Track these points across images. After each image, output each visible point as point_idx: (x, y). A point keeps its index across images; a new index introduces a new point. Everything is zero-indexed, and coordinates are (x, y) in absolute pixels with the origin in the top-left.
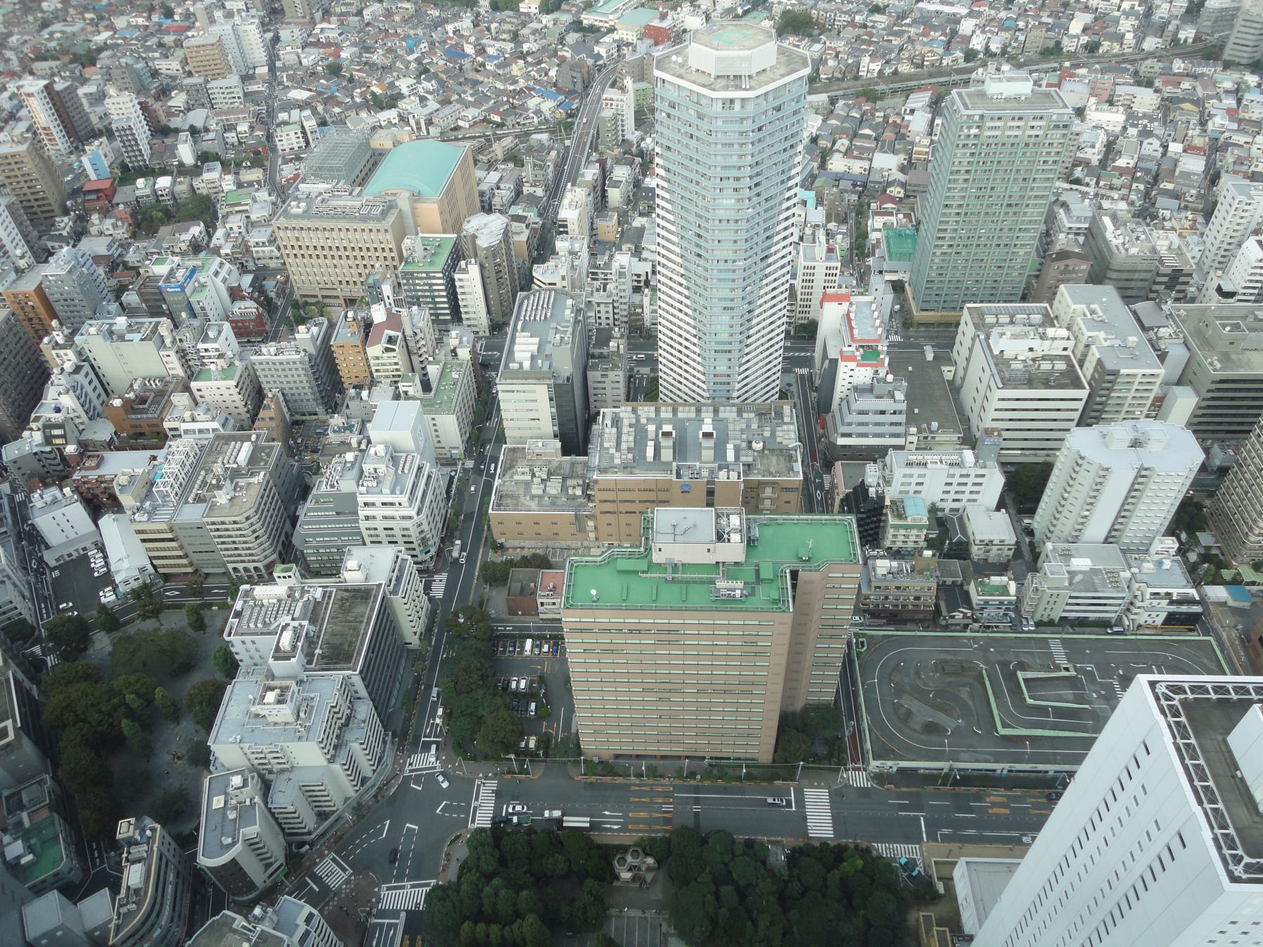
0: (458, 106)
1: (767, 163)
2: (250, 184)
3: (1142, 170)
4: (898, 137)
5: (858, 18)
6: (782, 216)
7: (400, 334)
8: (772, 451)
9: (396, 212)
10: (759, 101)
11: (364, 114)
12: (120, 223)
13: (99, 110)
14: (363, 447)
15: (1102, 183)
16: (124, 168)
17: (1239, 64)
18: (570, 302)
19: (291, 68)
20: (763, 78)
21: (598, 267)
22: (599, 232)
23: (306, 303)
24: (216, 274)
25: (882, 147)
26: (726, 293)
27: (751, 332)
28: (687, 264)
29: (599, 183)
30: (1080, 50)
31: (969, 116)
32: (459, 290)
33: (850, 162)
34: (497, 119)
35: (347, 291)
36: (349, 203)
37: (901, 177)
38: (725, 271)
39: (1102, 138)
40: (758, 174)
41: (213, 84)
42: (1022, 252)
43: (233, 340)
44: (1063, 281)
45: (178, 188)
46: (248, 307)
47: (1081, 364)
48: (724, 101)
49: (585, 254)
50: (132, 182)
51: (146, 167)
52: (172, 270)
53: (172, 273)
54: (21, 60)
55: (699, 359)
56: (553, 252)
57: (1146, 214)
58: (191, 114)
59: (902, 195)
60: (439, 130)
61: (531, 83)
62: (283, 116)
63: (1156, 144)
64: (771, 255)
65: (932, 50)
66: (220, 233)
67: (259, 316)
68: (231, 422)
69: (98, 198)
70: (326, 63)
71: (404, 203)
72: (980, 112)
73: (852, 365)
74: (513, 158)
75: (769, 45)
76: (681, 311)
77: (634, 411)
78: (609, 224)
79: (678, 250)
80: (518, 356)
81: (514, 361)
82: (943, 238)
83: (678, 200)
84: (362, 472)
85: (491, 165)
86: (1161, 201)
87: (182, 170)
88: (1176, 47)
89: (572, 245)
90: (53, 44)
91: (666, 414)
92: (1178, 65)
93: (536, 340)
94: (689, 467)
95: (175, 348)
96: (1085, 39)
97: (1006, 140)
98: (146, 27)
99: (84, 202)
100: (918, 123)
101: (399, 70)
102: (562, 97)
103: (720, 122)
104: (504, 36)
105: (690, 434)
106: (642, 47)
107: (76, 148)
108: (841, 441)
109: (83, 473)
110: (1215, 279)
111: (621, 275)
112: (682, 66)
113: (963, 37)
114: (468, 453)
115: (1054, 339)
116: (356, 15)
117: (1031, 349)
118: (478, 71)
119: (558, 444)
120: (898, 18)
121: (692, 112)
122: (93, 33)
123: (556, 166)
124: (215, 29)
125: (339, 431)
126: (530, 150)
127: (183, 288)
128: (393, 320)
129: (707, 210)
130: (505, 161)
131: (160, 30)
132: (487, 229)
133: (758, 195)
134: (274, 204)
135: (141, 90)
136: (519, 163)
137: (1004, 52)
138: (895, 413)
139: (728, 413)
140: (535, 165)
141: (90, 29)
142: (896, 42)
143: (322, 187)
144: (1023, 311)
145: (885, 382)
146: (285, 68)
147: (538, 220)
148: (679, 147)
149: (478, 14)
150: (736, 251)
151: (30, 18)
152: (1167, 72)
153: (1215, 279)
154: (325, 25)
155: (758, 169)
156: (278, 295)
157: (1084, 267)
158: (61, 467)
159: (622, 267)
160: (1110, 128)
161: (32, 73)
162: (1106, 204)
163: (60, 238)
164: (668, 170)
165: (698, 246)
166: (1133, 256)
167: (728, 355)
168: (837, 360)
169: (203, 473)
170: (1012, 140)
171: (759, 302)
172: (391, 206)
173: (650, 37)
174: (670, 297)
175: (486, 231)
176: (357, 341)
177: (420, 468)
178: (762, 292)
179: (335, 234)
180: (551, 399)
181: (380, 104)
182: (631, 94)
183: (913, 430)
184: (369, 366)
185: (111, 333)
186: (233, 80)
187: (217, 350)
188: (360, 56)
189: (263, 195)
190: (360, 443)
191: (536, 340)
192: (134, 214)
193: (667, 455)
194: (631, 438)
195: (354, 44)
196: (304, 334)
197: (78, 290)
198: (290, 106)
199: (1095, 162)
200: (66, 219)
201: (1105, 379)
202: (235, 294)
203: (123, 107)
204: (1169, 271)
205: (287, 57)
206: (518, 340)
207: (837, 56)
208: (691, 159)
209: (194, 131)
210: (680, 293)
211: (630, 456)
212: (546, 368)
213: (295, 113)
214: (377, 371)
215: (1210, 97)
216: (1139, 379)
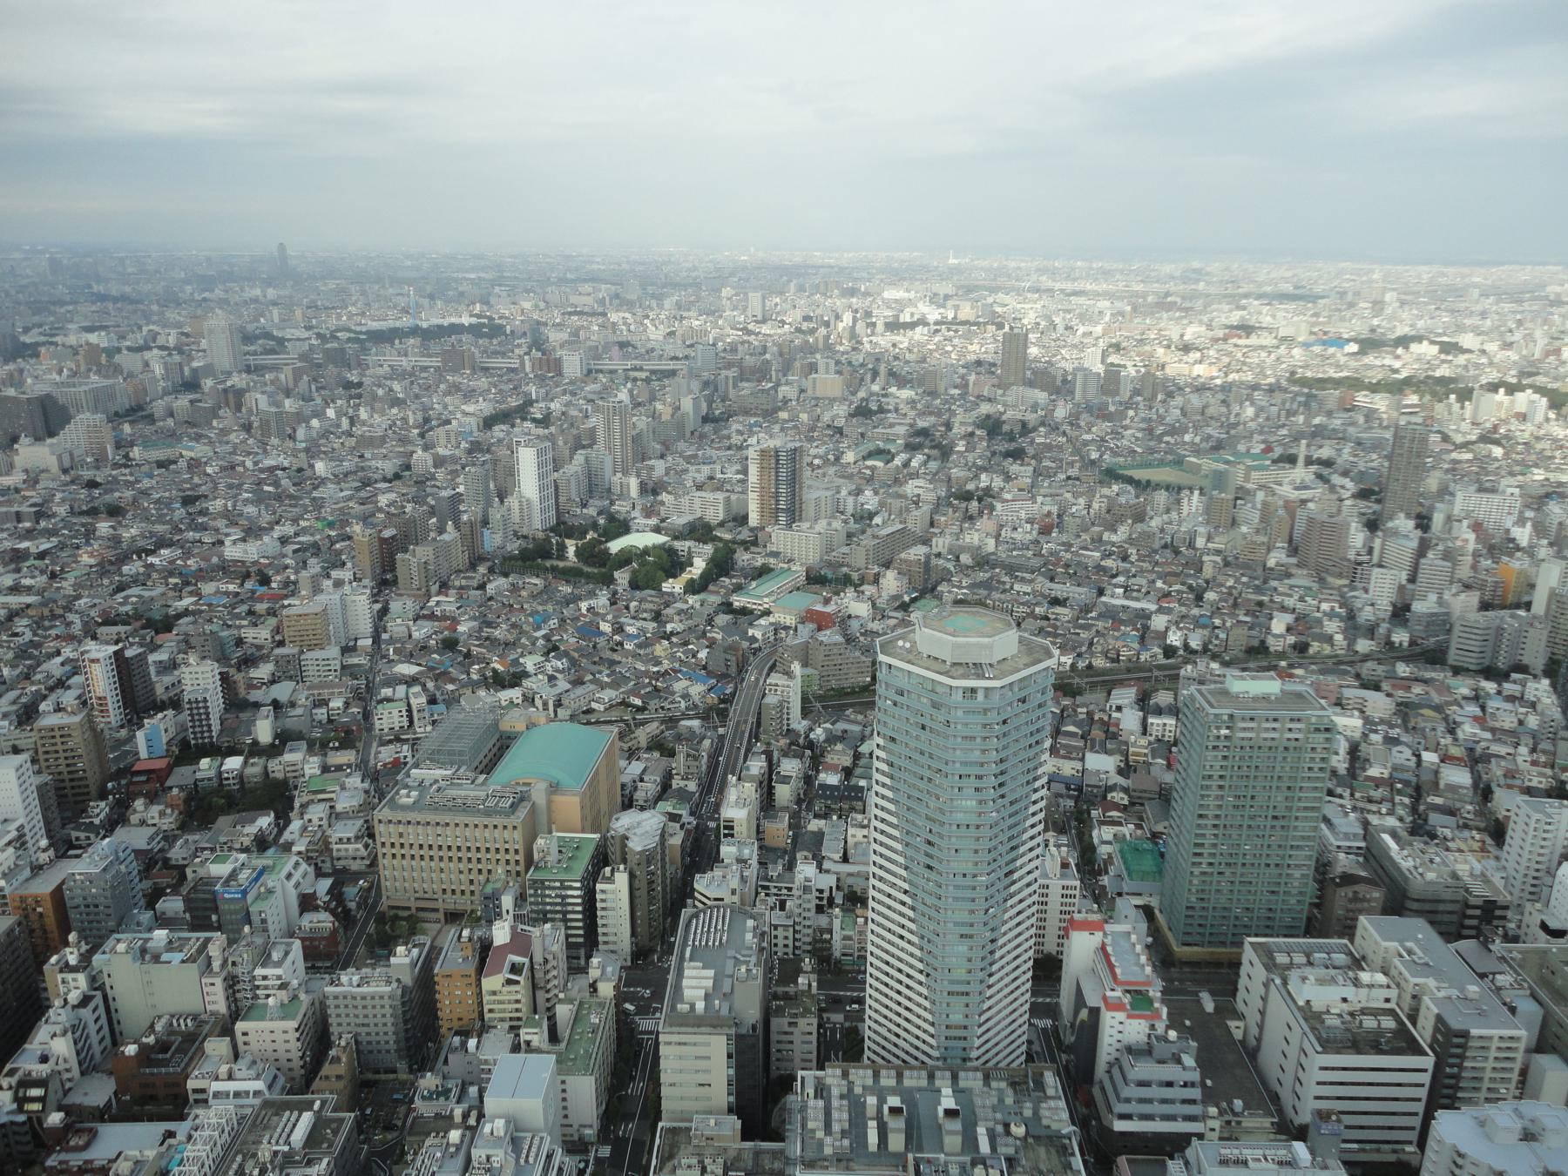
0: (592, 687)
1: (1013, 760)
2: (339, 768)
4: (1109, 737)
6: (1029, 823)
7: (526, 960)
8: (1037, 1138)
11: (482, 693)
12: (169, 811)
13: (168, 680)
14: (472, 1121)
15: (1357, 795)
16: (184, 744)
17: (1468, 670)
18: (750, 923)
20: (1005, 666)
23: (396, 918)
24: (289, 876)
26: (964, 916)
27: (995, 968)
28: (912, 877)
30: (1289, 650)
32: (599, 905)
34: (638, 702)
35: (450, 903)
36: (473, 794)
37: (1120, 780)
38: (964, 887)
40: (1002, 773)
43: (301, 964)
44: (1361, 911)
45: (250, 771)
46: (322, 921)
47: (1413, 1019)
49: (754, 862)
50: (195, 760)
51: (212, 744)
52: (234, 870)
53: (233, 875)
54: (85, 624)
55: (927, 1004)
57: (1420, 829)
58: (276, 686)
60: (569, 712)
61: (677, 665)
62: (386, 692)
63: (1408, 753)
64: (1015, 870)
66: (296, 825)
67: (334, 932)
68: (281, 1081)
69: (148, 781)
71: (539, 794)
73: (1121, 1016)
74: (659, 746)
76: (902, 937)
77: (845, 1075)
78: (779, 826)
80: (687, 993)
81: (683, 1002)
82: (1200, 854)
83: (903, 800)
84: (468, 1160)
85: (632, 754)
87: (255, 750)
88: (1391, 652)
91: (888, 1080)
92: (1403, 669)
93: (711, 973)
94: (929, 1161)
95: (224, 974)
96: (1291, 639)
97: (1262, 743)
98: (237, 594)
99: (128, 785)
100: (1129, 720)
101: (524, 646)
102: (714, 681)
103: (960, 713)
105: (922, 1110)
107: (129, 721)
108: (1120, 1126)
109: (63, 1156)
110: (1535, 913)
111: (806, 889)
112: (909, 651)
113: (1157, 632)
114: (604, 1135)
115: (1371, 986)
117: (1345, 1000)
119: (735, 1123)
121: (924, 700)
125: (430, 1098)
126: (679, 738)
127: (245, 893)
128: (520, 942)
129: (942, 811)
130: (649, 749)
132: (642, 829)
133: (1002, 796)
134: (367, 792)
135: (222, 659)
137: (1205, 650)
138: (1185, 1085)
139: (973, 1081)
141: (171, 593)
142: (1084, 635)
144: (1321, 949)
145: (1166, 1040)
146: (391, 641)
147: (691, 819)
148: (906, 739)
149: (615, 593)
150: (976, 864)
151: (106, 581)
152: (1391, 676)
153: (1535, 913)
155: (1003, 767)
156: (359, 906)
158: (29, 1148)
159: (808, 880)
160: (1348, 733)
161: (94, 637)
163: (90, 827)
164: (891, 765)
165: (927, 855)
166: (1430, 883)
167: (965, 999)
168: (1098, 1009)
169: (239, 1158)
170: (1269, 743)
171: (1003, 929)
172: (523, 798)
173: (812, 620)
174: (887, 918)
176: (471, 969)
177: (549, 1157)
178: (1007, 916)
179: (449, 831)
180: (729, 1056)
181: (500, 682)
183: (1213, 1111)
184: (481, 1004)
185: (143, 951)
186: (333, 651)
187: (279, 977)
189: (355, 781)
190: (466, 1116)
191: (711, 973)
192: (187, 801)
193: (896, 1142)
194: (845, 1116)
195: (474, 618)
196: (402, 956)
197: (108, 894)
198: (394, 681)
200: (102, 804)
201: (1451, 1044)
202: (307, 903)
203: (200, 678)
204: (1479, 902)
206: (687, 973)
208: (922, 753)
209: (276, 704)
210: (903, 915)
211: (846, 1142)
212: (724, 1012)
213: (401, 690)
214: (491, 1011)
215: (1449, 704)
216: (1496, 1043)
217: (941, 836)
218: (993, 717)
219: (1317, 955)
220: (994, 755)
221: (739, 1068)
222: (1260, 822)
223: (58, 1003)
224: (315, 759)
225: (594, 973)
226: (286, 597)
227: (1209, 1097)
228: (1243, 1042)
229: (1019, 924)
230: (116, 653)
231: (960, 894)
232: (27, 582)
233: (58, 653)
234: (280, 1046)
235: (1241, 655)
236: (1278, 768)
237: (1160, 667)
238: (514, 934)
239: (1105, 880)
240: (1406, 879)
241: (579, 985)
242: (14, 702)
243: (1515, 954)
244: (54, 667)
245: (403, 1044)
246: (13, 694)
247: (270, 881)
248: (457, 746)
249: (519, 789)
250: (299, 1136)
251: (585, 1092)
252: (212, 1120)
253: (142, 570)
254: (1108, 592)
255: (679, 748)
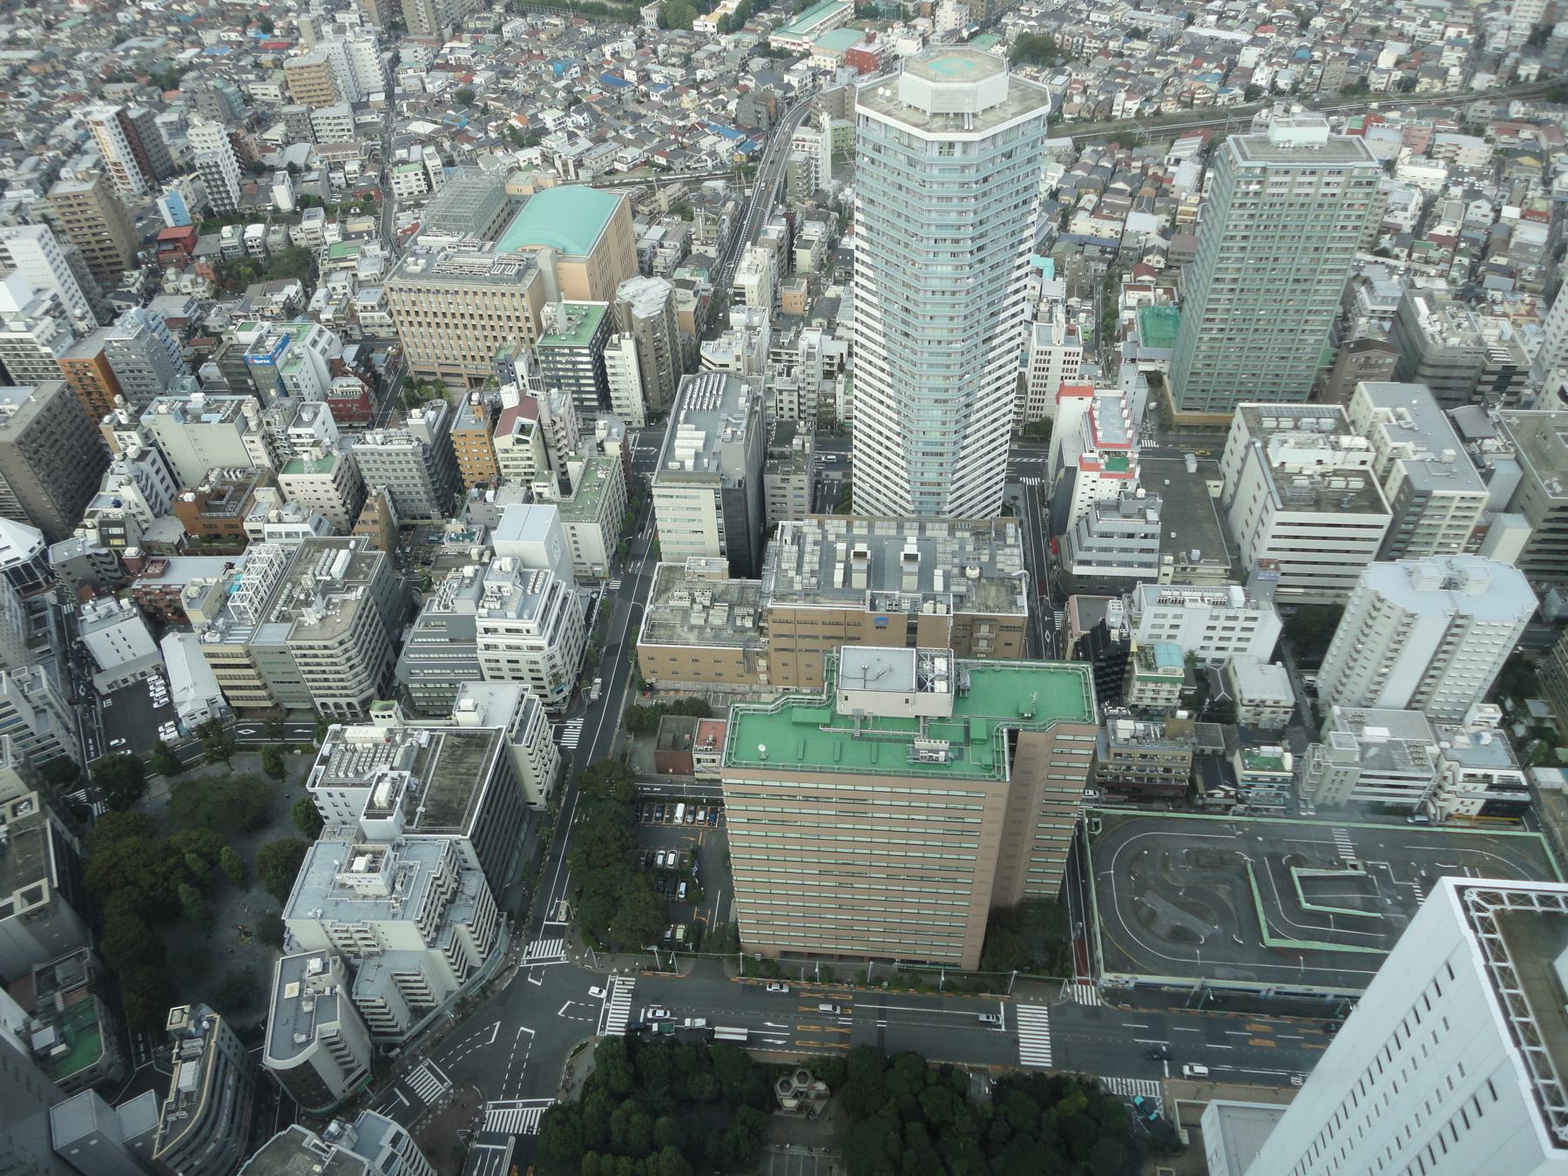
0: (615, 145)
2: (359, 235)
3: (1467, 240)
4: (1159, 193)
5: (1112, 45)
7: (535, 422)
9: (534, 272)
10: (984, 145)
11: (499, 153)
12: (200, 280)
13: (180, 142)
14: (485, 559)
15: (1415, 256)
16: (208, 213)
18: (745, 388)
19: (412, 95)
20: (990, 116)
21: (782, 347)
22: (783, 303)
23: (422, 382)
25: (1139, 205)
26: (940, 383)
27: (969, 431)
28: (892, 345)
29: (786, 242)
31: (1248, 169)
32: (609, 371)
33: (1099, 223)
34: (662, 161)
35: (473, 368)
37: (1162, 243)
38: (938, 354)
39: (1417, 199)
40: (982, 236)
41: (318, 113)
42: (1311, 339)
44: (1363, 377)
45: (272, 238)
46: (352, 385)
47: (1383, 481)
48: (942, 145)
49: (765, 330)
51: (234, 212)
52: (261, 337)
53: (260, 342)
54: (90, 81)
55: (903, 463)
56: (726, 325)
57: (1471, 295)
58: (290, 149)
59: (1162, 265)
60: (590, 173)
61: (705, 118)
62: (401, 153)
63: (1486, 207)
64: (996, 336)
65: (1204, 86)
66: (320, 293)
67: (365, 396)
68: (326, 524)
69: (176, 249)
70: (455, 89)
71: (544, 262)
72: (1262, 164)
73: (1095, 475)
74: (681, 209)
75: (999, 76)
76: (882, 402)
77: (821, 525)
78: (797, 293)
79: (880, 327)
80: (678, 452)
82: (1213, 320)
83: (882, 266)
84: (482, 590)
85: (653, 218)
86: (1491, 280)
87: (277, 216)
88: (1515, 86)
89: (750, 317)
90: (128, 63)
92: (1517, 109)
93: (702, 434)
95: (261, 433)
96: (1398, 75)
97: (1293, 199)
99: (157, 253)
100: (1184, 176)
101: (544, 99)
102: (743, 136)
103: (936, 171)
104: (674, 60)
105: (888, 554)
106: (843, 77)
107: (152, 188)
108: (1078, 570)
109: (145, 581)
111: (810, 356)
112: (890, 100)
114: (614, 570)
115: (1349, 449)
116: (494, 32)
117: (1320, 462)
118: (640, 103)
119: (725, 563)
120: (1162, 45)
121: (901, 157)
122: (176, 50)
123: (733, 221)
124: (323, 47)
125: (457, 540)
126: (702, 201)
127: (273, 359)
128: (527, 405)
129: (917, 277)
130: (671, 213)
131: (257, 47)
133: (981, 261)
135: (231, 119)
136: (688, 216)
137: (1295, 89)
138: (1146, 537)
139: (937, 531)
140: (707, 219)
141: (173, 45)
142: (1159, 74)
143: (446, 240)
144: (1311, 414)
145: (1135, 497)
147: (709, 286)
149: (643, 33)
150: (952, 330)
151: (103, 32)
152: (1502, 117)
154: (455, 44)
155: (981, 230)
156: (388, 371)
157: (1389, 360)
158: (119, 574)
160: (1427, 187)
161: (102, 97)
162: (1420, 282)
163: (128, 296)
164: (870, 228)
165: (905, 322)
166: (1453, 348)
167: (939, 459)
169: (289, 585)
170: (1301, 200)
171: (980, 394)
172: (529, 266)
174: (869, 385)
175: (644, 298)
176: (483, 428)
177: (554, 588)
178: (983, 382)
179: (459, 298)
180: (718, 508)
181: (520, 140)
182: (828, 134)
185: (184, 412)
186: (343, 108)
187: (312, 436)
188: (497, 82)
189: (374, 249)
190: (481, 555)
191: (702, 434)
192: (217, 269)
193: (859, 580)
194: (816, 559)
195: (490, 68)
197: (147, 359)
199: (1407, 229)
200: (136, 274)
201: (1413, 501)
202: (336, 368)
203: (208, 140)
204: (1498, 368)
205: (409, 82)
206: (679, 434)
207: (1085, 91)
208: (899, 215)
209: (293, 170)
210: (881, 380)
211: (814, 580)
212: (713, 469)
213: (416, 150)
216: (1456, 503)
217: (916, 303)
218: (971, 175)
219: (1305, 420)
220: (970, 218)
221: (727, 517)
222: (1279, 285)
223: (116, 456)
224: (333, 226)
225: (600, 434)
226: (291, 46)
227: (1167, 545)
228: (1218, 501)
229: (998, 389)
230: (118, 114)
231: (934, 360)
232: (23, 33)
233: (70, 116)
234: (324, 496)
235: (1334, 96)
236: (1308, 228)
237: (1238, 112)
238: (522, 396)
239: (1121, 347)
240: (1425, 344)
241: (586, 449)
242: (34, 169)
243: (1514, 420)
244: (67, 130)
245: (432, 494)
246: (31, 161)
247: (297, 347)
248: (458, 211)
249: (526, 255)
250: (338, 569)
251: (593, 540)
252: (262, 555)
253: (138, 17)
254: (1198, 21)
255: (697, 211)
